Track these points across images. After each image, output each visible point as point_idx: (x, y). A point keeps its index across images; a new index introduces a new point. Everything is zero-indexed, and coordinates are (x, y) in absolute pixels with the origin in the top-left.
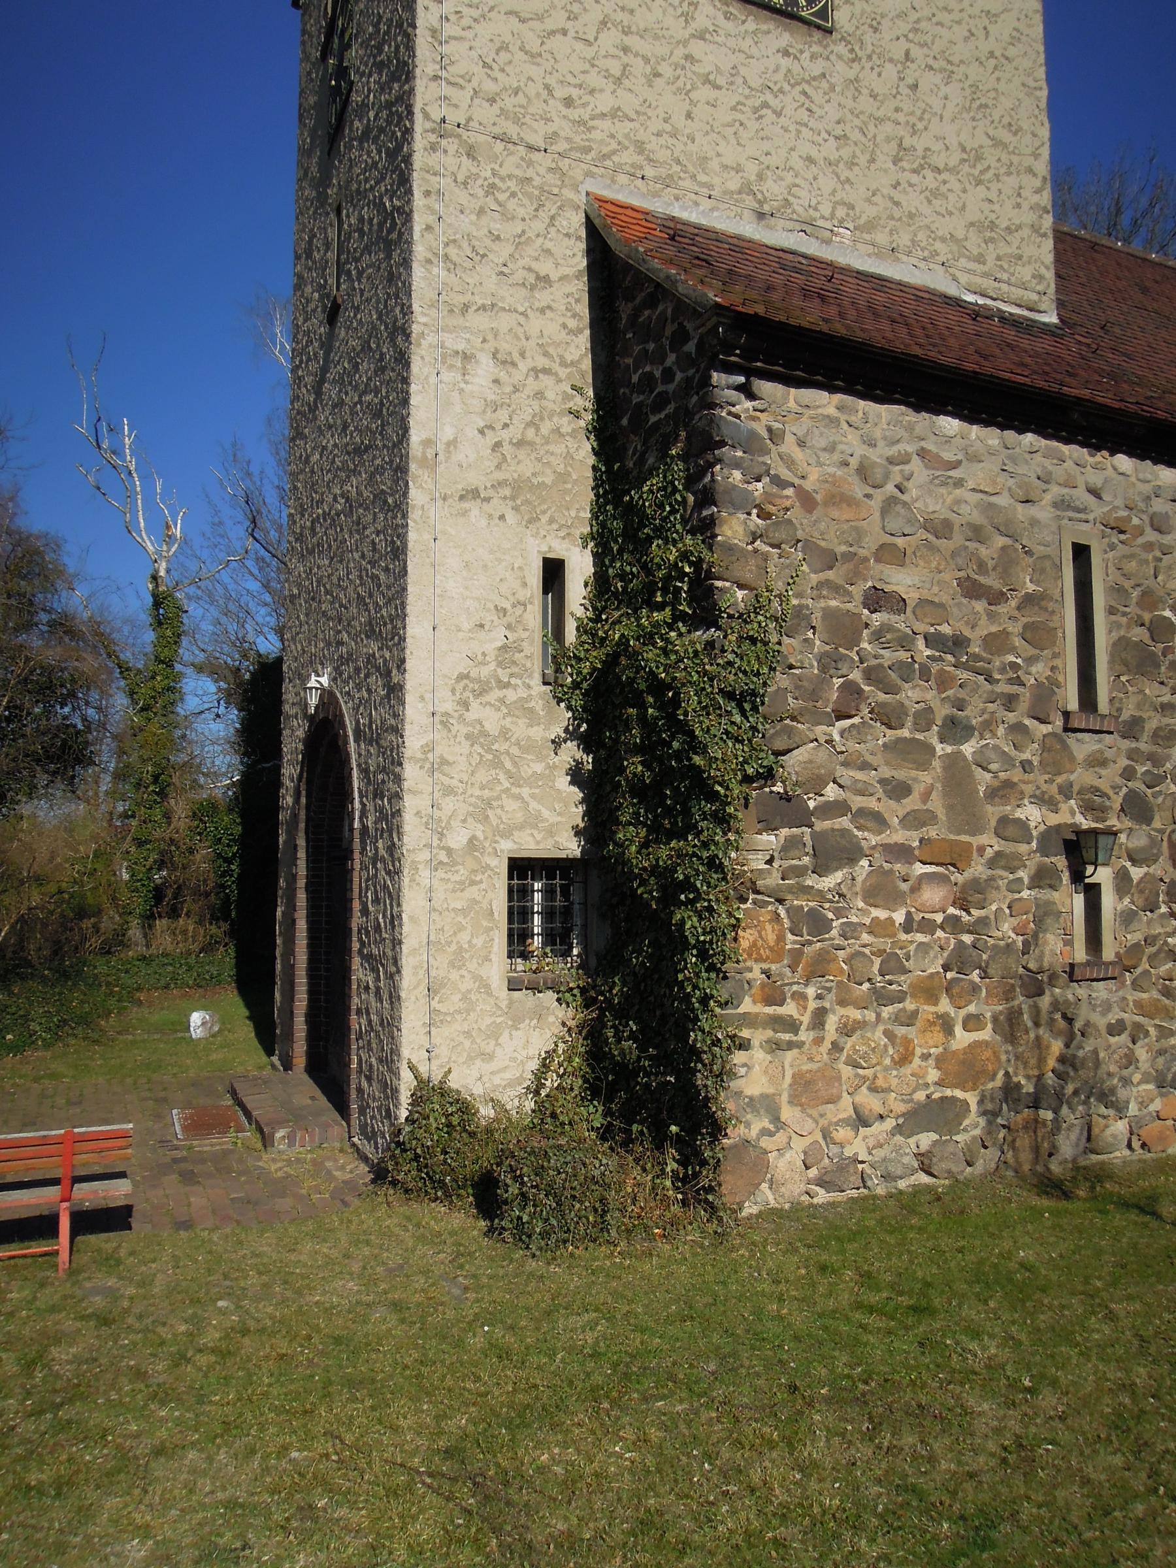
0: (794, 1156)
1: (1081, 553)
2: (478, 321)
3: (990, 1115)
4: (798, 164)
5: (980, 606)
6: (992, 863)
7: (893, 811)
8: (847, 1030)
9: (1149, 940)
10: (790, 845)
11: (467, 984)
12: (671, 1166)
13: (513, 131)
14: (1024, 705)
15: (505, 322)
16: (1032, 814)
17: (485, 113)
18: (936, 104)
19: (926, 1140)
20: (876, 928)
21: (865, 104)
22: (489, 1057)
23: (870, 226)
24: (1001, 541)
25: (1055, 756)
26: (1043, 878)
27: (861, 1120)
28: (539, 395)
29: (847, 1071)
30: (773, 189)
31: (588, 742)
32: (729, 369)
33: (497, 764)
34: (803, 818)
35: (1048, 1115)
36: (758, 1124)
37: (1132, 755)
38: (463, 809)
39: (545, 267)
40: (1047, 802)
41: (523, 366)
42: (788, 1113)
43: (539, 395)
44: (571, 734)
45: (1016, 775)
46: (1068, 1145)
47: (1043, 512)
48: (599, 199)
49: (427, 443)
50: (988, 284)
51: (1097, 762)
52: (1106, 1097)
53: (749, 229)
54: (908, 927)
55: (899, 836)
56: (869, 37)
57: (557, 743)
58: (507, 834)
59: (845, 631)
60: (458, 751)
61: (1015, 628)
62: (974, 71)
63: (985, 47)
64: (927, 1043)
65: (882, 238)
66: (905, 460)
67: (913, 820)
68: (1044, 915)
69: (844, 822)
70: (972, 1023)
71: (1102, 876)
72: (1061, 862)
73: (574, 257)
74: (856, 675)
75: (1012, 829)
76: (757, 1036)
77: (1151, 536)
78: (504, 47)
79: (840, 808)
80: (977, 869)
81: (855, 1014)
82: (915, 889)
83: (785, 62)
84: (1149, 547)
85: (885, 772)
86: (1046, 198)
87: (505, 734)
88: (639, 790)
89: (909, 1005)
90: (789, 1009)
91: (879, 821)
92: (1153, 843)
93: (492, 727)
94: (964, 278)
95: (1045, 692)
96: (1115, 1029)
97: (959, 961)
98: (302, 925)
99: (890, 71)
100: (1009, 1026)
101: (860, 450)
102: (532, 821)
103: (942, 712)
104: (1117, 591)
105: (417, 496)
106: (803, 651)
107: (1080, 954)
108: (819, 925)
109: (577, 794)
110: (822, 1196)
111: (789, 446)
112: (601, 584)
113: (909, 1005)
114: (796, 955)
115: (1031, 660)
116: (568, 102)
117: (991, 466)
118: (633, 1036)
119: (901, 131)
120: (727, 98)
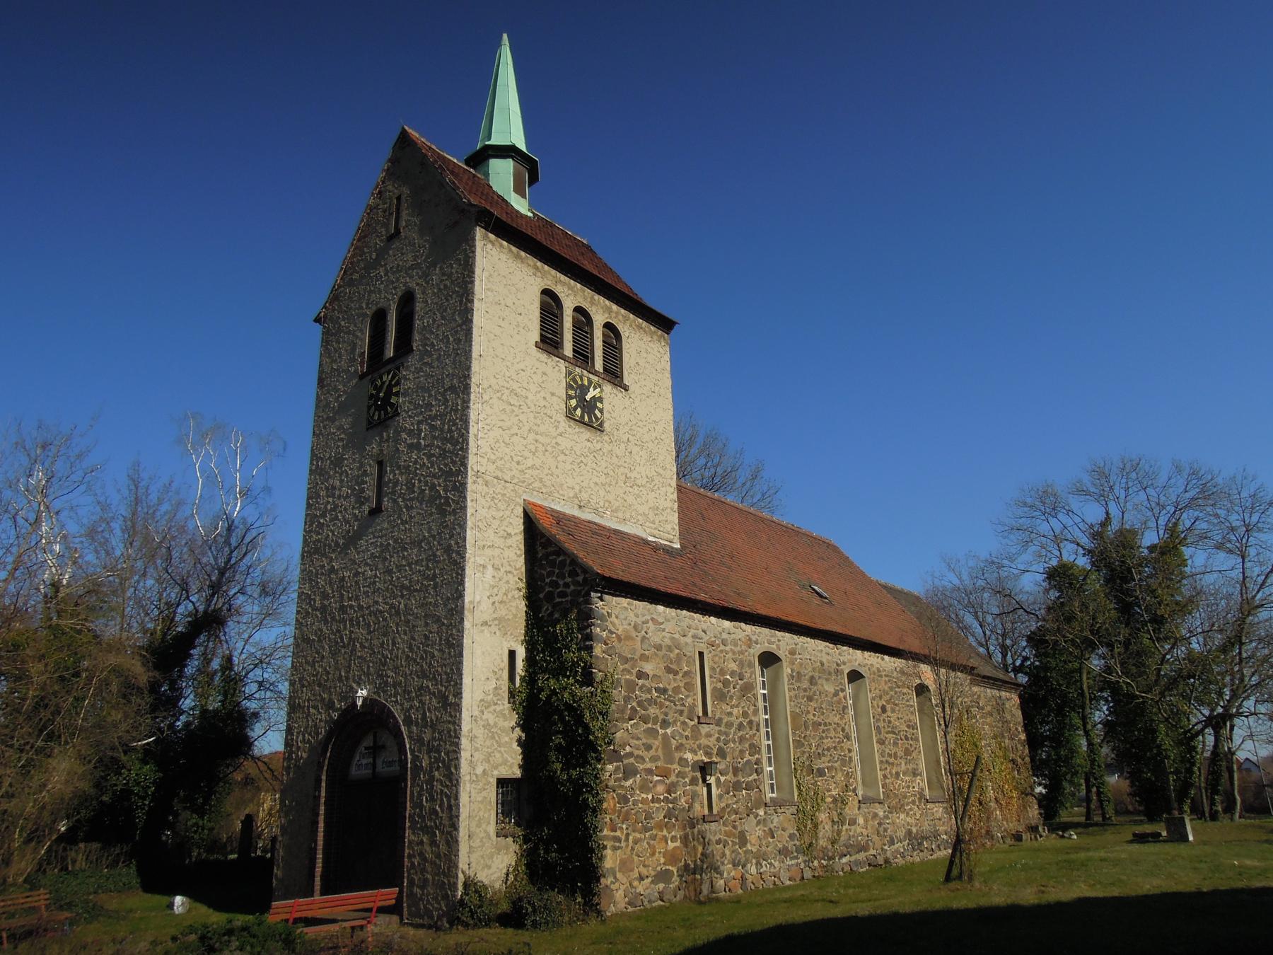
0: (621, 893)
1: (701, 654)
2: (488, 552)
3: (681, 876)
4: (592, 485)
5: (671, 676)
6: (677, 776)
7: (647, 755)
8: (636, 842)
9: (727, 806)
10: (617, 769)
11: (482, 835)
12: (579, 899)
13: (500, 475)
14: (685, 713)
15: (497, 552)
16: (689, 756)
17: (491, 468)
18: (638, 458)
19: (661, 886)
20: (644, 801)
21: (615, 460)
22: (489, 867)
23: (616, 510)
24: (677, 651)
25: (696, 733)
26: (693, 782)
27: (641, 878)
28: (508, 582)
29: (636, 858)
30: (585, 496)
31: (523, 729)
32: (597, 591)
33: (493, 738)
34: (620, 759)
35: (698, 877)
36: (611, 879)
37: (720, 732)
38: (482, 757)
39: (510, 530)
40: (694, 752)
41: (502, 570)
42: (619, 875)
43: (508, 582)
44: (518, 725)
45: (684, 741)
46: (705, 889)
47: (689, 640)
48: (530, 503)
49: (471, 602)
50: (656, 532)
51: (709, 735)
52: (717, 870)
53: (576, 512)
54: (653, 801)
55: (648, 766)
56: (616, 433)
57: (513, 729)
58: (496, 768)
59: (631, 686)
60: (480, 732)
61: (682, 685)
62: (650, 445)
63: (654, 435)
64: (660, 848)
65: (620, 515)
66: (646, 622)
67: (654, 759)
68: (694, 796)
69: (632, 760)
70: (674, 839)
71: (711, 780)
72: (699, 774)
73: (518, 526)
74: (634, 704)
75: (683, 762)
76: (609, 844)
77: (722, 647)
78: (498, 441)
79: (630, 755)
80: (673, 778)
81: (638, 836)
82: (655, 786)
83: (589, 444)
84: (721, 651)
85: (644, 741)
86: (675, 496)
87: (496, 724)
88: (559, 748)
89: (654, 832)
90: (618, 833)
91: (641, 759)
92: (727, 767)
93: (491, 722)
94: (648, 530)
95: (692, 708)
96: (718, 842)
97: (668, 815)
98: (321, 825)
99: (623, 446)
100: (685, 840)
101: (634, 619)
102: (505, 762)
103: (661, 717)
104: (713, 669)
105: (467, 624)
106: (618, 694)
107: (706, 812)
108: (626, 800)
109: (519, 750)
110: (630, 909)
111: (613, 618)
112: (530, 660)
113: (654, 832)
114: (620, 812)
115: (687, 696)
116: (518, 463)
117: (673, 623)
118: (556, 851)
119: (627, 471)
120: (570, 459)
